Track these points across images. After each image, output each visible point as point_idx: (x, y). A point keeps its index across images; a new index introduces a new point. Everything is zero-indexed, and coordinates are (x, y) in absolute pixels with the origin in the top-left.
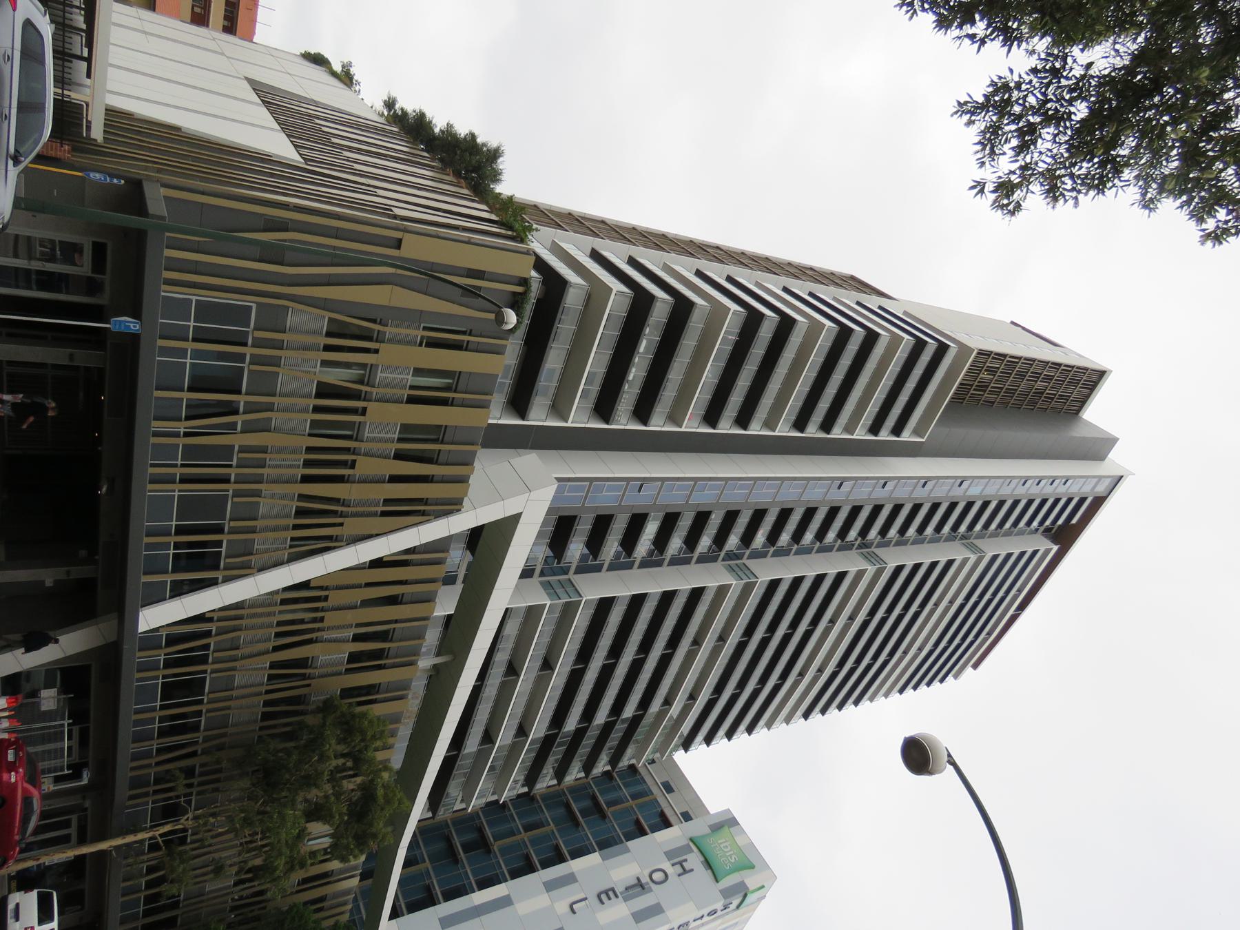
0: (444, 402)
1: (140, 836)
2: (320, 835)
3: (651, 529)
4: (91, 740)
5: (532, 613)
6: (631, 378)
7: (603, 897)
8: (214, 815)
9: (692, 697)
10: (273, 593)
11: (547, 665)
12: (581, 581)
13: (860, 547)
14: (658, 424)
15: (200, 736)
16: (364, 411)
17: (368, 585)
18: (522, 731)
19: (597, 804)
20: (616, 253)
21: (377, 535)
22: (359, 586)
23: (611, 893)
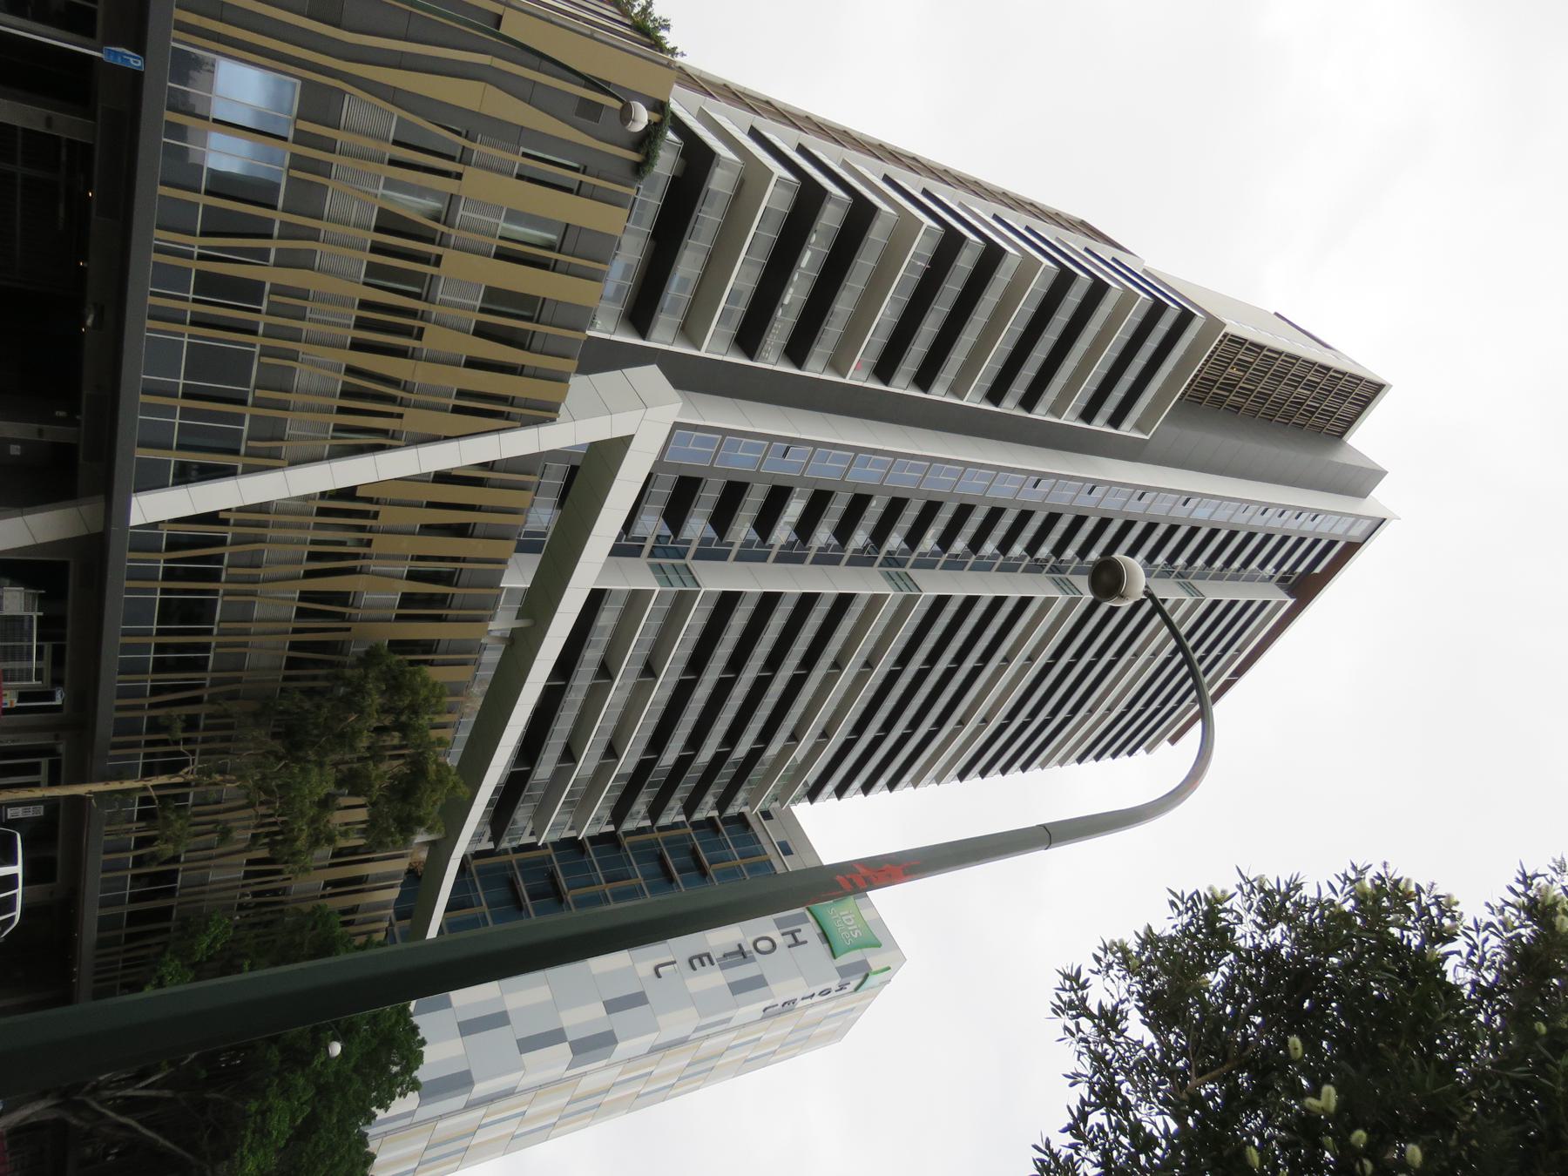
0: (542, 264)
1: (128, 784)
2: (351, 815)
3: (794, 509)
5: (636, 600)
6: (786, 301)
7: (696, 962)
8: (222, 772)
9: (826, 734)
10: (307, 498)
11: (650, 670)
12: (701, 569)
13: (1051, 571)
14: (815, 369)
15: (207, 677)
16: (437, 261)
17: (431, 505)
18: (612, 752)
19: (697, 859)
20: (784, 138)
21: (447, 438)
22: (419, 505)
23: (705, 959)
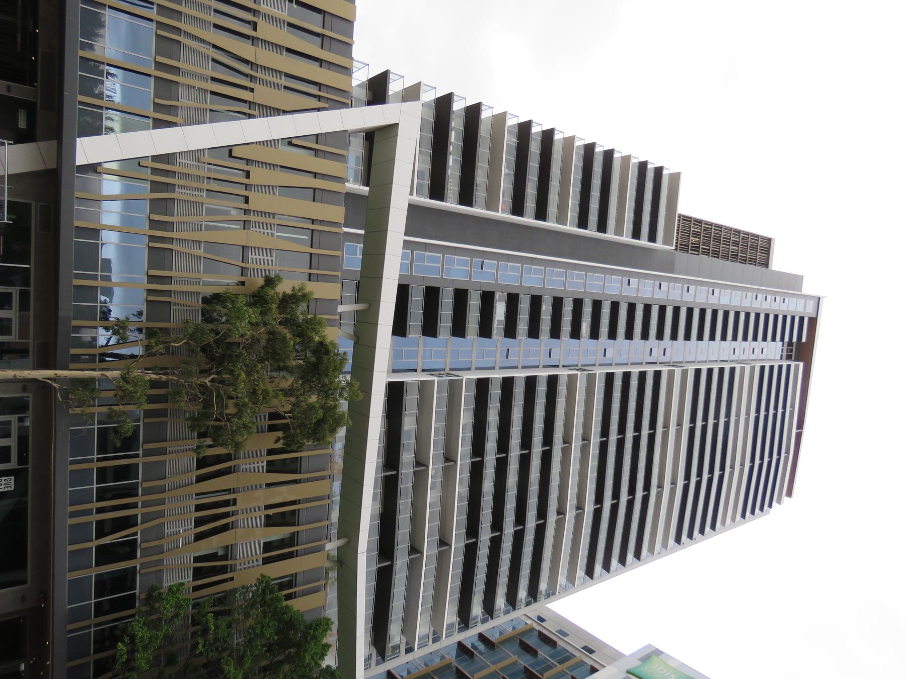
4: (30, 492)
11: (449, 458)
21: (285, 112)
